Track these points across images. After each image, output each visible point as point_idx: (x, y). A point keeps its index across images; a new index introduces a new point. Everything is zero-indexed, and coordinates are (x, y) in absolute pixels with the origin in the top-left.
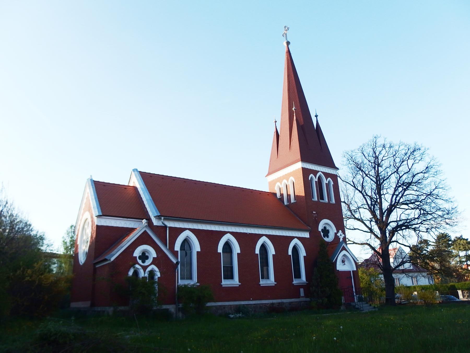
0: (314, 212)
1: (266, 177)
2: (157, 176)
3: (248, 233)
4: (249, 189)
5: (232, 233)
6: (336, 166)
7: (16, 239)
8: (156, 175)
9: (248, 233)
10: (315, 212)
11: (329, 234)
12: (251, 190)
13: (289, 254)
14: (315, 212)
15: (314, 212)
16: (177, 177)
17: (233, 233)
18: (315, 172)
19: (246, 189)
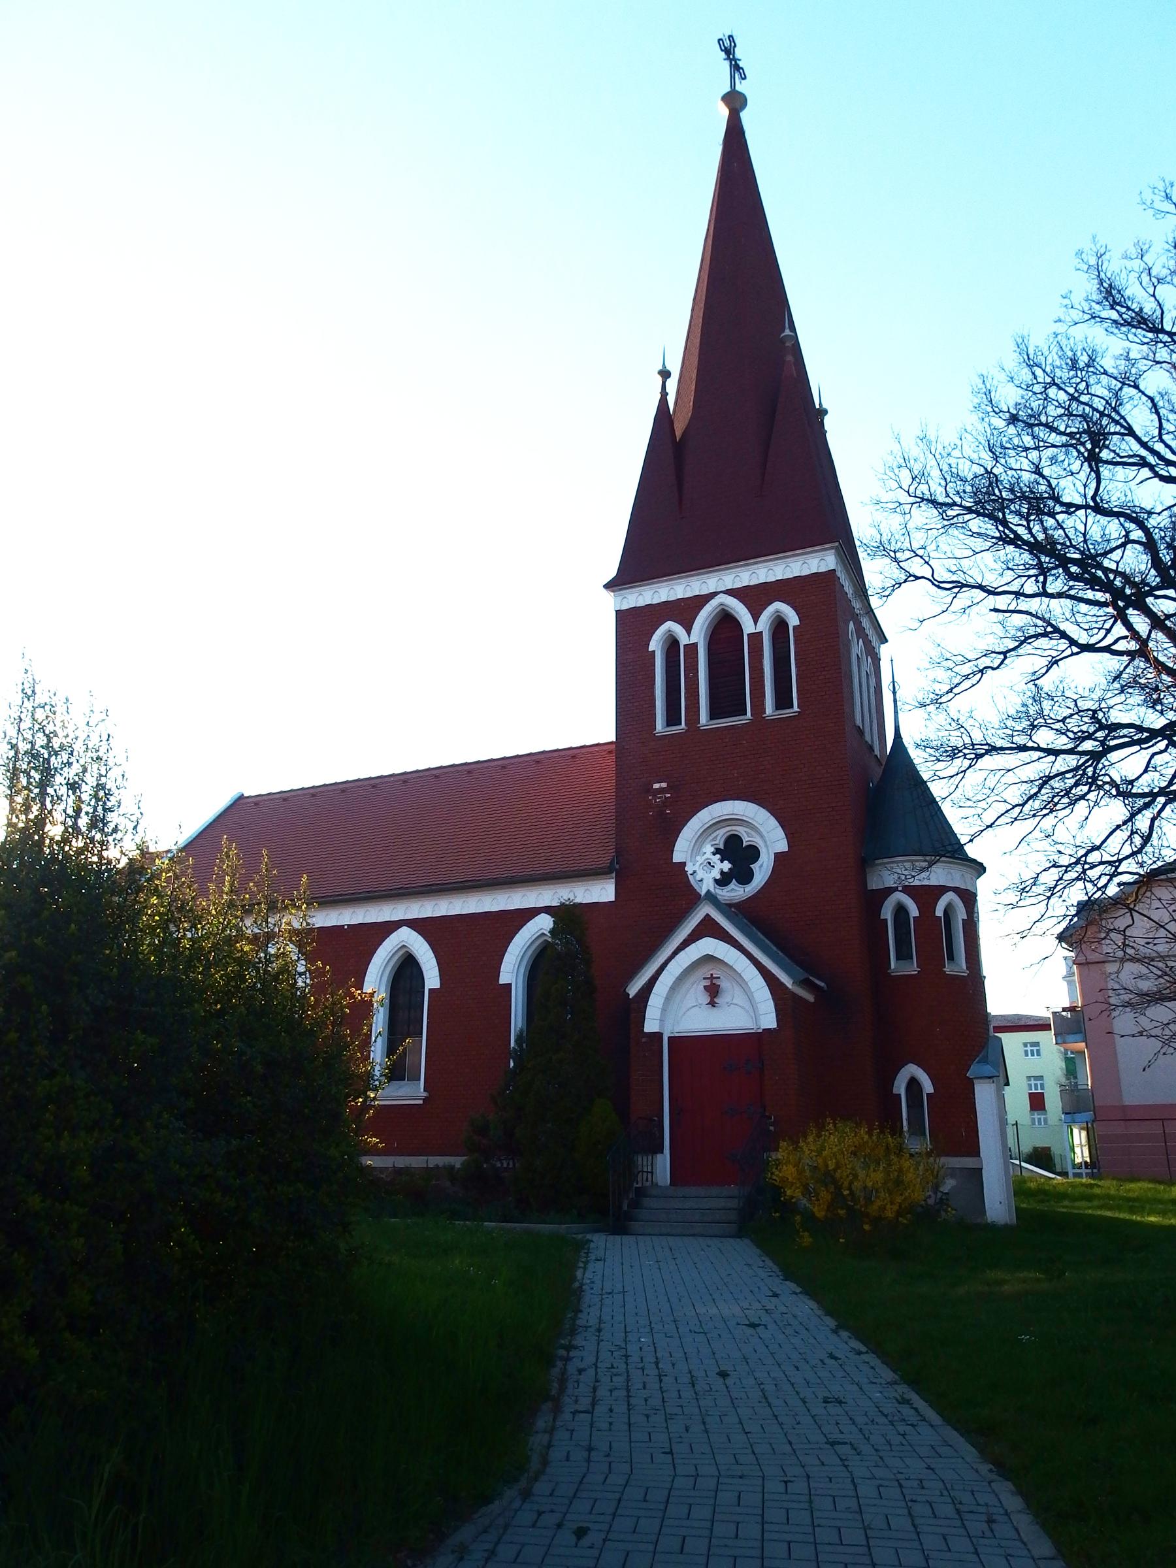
0: (656, 786)
1: (991, 610)
2: (415, 775)
3: (346, 927)
4: (492, 760)
5: (414, 924)
6: (614, 574)
7: (313, 981)
8: (563, 753)
9: (346, 927)
10: (664, 785)
11: (754, 866)
12: (402, 777)
13: (438, 986)
14: (664, 785)
15: (656, 786)
16: (547, 749)
17: (416, 924)
18: (685, 610)
19: (479, 762)
